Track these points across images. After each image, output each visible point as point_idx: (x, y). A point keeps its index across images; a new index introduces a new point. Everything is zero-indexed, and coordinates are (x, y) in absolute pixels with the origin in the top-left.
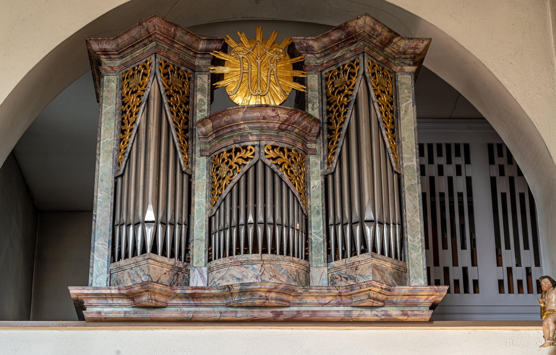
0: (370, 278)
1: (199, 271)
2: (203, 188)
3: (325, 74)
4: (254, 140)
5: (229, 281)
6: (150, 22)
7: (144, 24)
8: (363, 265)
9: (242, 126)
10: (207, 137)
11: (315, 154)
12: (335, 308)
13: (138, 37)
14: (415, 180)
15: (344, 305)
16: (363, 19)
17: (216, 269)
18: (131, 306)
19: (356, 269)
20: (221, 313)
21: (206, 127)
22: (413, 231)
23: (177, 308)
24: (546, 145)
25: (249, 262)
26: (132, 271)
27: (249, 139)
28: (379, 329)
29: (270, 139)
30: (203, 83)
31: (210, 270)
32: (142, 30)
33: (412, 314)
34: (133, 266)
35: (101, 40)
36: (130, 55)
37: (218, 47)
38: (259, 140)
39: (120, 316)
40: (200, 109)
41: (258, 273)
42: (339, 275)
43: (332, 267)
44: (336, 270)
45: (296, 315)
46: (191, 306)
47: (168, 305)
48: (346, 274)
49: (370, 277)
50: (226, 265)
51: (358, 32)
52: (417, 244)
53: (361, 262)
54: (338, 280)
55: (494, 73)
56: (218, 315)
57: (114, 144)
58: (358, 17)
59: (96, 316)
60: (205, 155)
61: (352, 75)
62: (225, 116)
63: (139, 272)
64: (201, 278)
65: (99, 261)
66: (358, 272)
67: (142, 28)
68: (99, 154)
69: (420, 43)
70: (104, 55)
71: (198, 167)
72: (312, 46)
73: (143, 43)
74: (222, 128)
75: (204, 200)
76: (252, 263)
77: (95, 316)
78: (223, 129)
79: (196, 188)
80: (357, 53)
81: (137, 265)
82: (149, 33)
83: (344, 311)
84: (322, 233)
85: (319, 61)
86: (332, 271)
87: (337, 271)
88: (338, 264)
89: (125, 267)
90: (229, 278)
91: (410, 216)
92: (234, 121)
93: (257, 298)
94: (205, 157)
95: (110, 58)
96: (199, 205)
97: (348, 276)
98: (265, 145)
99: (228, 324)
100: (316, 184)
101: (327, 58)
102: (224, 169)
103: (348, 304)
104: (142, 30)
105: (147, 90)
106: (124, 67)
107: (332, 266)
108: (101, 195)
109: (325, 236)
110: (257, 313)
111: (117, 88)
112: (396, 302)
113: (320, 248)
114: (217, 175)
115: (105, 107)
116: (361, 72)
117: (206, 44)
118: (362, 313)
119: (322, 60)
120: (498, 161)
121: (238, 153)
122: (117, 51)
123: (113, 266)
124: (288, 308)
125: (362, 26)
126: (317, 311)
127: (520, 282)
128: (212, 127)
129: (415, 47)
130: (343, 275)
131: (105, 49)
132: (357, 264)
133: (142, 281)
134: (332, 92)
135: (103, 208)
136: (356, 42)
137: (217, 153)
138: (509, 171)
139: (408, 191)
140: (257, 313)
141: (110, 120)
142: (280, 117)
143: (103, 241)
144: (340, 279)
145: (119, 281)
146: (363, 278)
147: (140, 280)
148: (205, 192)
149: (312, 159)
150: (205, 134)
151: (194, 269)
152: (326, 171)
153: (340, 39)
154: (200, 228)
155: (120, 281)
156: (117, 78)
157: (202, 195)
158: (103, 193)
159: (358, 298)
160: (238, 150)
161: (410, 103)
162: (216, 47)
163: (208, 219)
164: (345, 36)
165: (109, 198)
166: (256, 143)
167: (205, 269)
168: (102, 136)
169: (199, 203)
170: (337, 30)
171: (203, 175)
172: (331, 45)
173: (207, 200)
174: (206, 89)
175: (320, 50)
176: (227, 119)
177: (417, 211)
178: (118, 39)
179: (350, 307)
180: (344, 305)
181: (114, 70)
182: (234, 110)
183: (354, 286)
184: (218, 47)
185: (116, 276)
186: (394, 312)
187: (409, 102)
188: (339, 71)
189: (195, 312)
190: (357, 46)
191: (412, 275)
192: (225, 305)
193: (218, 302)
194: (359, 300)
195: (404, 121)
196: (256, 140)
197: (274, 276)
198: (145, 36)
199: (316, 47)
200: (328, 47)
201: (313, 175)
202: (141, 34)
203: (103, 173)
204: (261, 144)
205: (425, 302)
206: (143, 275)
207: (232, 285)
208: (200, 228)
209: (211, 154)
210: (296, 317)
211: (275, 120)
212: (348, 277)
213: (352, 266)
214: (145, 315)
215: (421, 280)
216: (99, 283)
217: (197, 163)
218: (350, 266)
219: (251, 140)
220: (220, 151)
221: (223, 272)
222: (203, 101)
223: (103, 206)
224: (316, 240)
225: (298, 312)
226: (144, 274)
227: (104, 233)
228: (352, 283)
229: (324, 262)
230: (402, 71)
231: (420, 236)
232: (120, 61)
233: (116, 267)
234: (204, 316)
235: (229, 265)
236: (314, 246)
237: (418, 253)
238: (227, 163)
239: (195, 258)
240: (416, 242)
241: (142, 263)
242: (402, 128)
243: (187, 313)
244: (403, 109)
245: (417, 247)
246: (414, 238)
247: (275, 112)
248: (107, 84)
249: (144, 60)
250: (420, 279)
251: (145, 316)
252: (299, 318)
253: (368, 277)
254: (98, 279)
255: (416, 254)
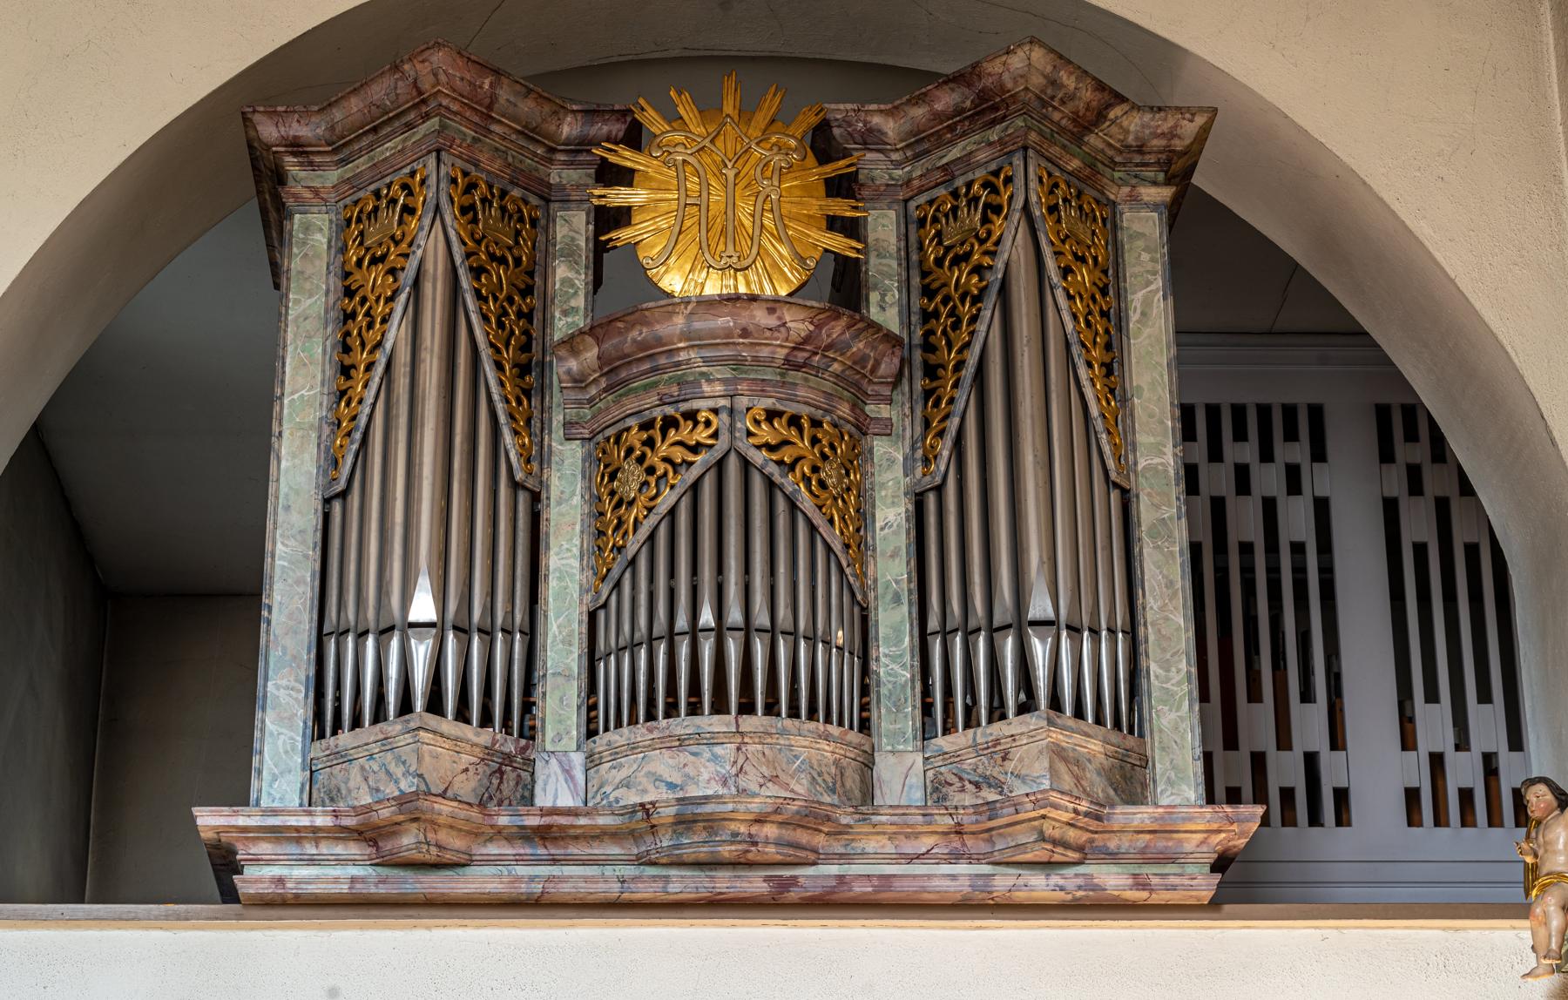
0: (1042, 784)
1: (560, 762)
2: (573, 529)
3: (917, 207)
4: (717, 394)
5: (645, 791)
6: (423, 62)
7: (407, 67)
8: (1025, 748)
9: (683, 356)
10: (583, 385)
11: (890, 435)
12: (946, 869)
13: (388, 103)
14: (1170, 506)
15: (969, 858)
16: (1022, 54)
17: (609, 758)
18: (368, 863)
19: (1004, 759)
20: (623, 882)
21: (582, 357)
22: (1164, 650)
23: (499, 868)
24: (1540, 410)
25: (703, 739)
26: (371, 762)
27: (703, 392)
28: (1068, 927)
29: (763, 391)
30: (572, 234)
31: (592, 761)
32: (400, 84)
33: (1162, 885)
34: (376, 751)
35: (286, 112)
36: (366, 156)
37: (614, 133)
38: (732, 393)
39: (337, 891)
40: (565, 307)
41: (728, 768)
42: (956, 775)
43: (937, 751)
44: (949, 761)
45: (835, 887)
46: (538, 861)
47: (474, 858)
48: (975, 771)
49: (1044, 781)
50: (638, 747)
51: (1009, 91)
52: (1175, 689)
53: (1017, 737)
54: (952, 788)
55: (1392, 207)
56: (616, 887)
57: (321, 404)
58: (1009, 47)
59: (270, 891)
60: (579, 436)
61: (992, 212)
62: (633, 326)
63: (392, 767)
64: (566, 782)
65: (279, 734)
66: (1010, 766)
67: (401, 79)
68: (280, 433)
69: (1186, 122)
70: (294, 154)
71: (558, 470)
72: (879, 131)
73: (404, 120)
74: (627, 360)
75: (576, 564)
76: (712, 741)
77: (267, 889)
78: (629, 363)
79: (552, 530)
80: (1008, 149)
81: (387, 748)
82: (420, 93)
83: (970, 875)
84: (908, 657)
85: (900, 172)
86: (936, 765)
87: (951, 763)
88: (952, 743)
89: (352, 752)
90: (646, 783)
91: (1155, 607)
92: (659, 341)
93: (724, 838)
94: (578, 442)
95: (311, 164)
96: (560, 579)
97: (980, 776)
98: (748, 409)
99: (642, 913)
100: (891, 518)
101: (923, 164)
102: (632, 476)
103: (981, 857)
104: (400, 84)
105: (414, 252)
106: (350, 189)
107: (936, 748)
108: (284, 549)
109: (917, 664)
110: (724, 883)
111: (329, 247)
112: (1116, 851)
113: (903, 700)
114: (612, 493)
115: (297, 302)
116: (1019, 203)
117: (580, 124)
118: (1021, 881)
119: (909, 168)
120: (1405, 452)
121: (672, 432)
122: (329, 145)
123: (318, 749)
124: (813, 868)
125: (1020, 72)
126: (894, 876)
127: (1466, 796)
128: (599, 358)
129: (1171, 133)
130: (968, 774)
131: (295, 137)
132: (1007, 743)
133: (400, 790)
134: (936, 259)
135: (292, 586)
136: (1004, 118)
137: (611, 432)
138: (1436, 482)
139: (1151, 537)
140: (724, 883)
141: (309, 337)
142: (788, 329)
143: (292, 679)
144: (960, 785)
145: (334, 793)
146: (1024, 782)
147: (394, 788)
148: (577, 541)
149: (880, 447)
150: (578, 377)
151: (547, 758)
152: (920, 481)
153: (959, 111)
154: (563, 642)
155: (339, 790)
156: (331, 221)
157: (568, 550)
158: (292, 542)
159: (1009, 839)
160: (670, 423)
161: (1157, 290)
162: (610, 131)
163: (585, 618)
164: (972, 102)
165: (306, 557)
166: (722, 402)
167: (578, 759)
168: (287, 383)
169: (561, 572)
170: (952, 85)
171: (573, 494)
172: (933, 128)
173: (585, 562)
174: (581, 250)
175: (902, 141)
176: (640, 334)
177: (1175, 593)
178: (334, 111)
179: (988, 863)
180: (971, 859)
181: (322, 198)
182: (661, 310)
183: (998, 805)
184: (614, 133)
185: (327, 777)
186: (1112, 879)
187: (1153, 287)
188: (957, 200)
189: (550, 879)
190: (1007, 128)
191: (1162, 775)
192: (634, 858)
193: (614, 850)
194: (1013, 844)
195: (1139, 340)
196: (722, 393)
197: (774, 779)
198: (408, 102)
199: (890, 133)
200: (924, 131)
201: (883, 493)
202: (397, 95)
203: (291, 488)
204: (736, 406)
205: (1199, 850)
206: (404, 775)
207: (653, 803)
208: (563, 642)
209: (594, 434)
210: (835, 892)
211: (777, 339)
212: (981, 780)
213: (993, 750)
214: (408, 886)
215: (1187, 789)
216: (280, 798)
217: (555, 459)
218: (988, 748)
219: (707, 395)
220: (620, 426)
221: (629, 767)
222: (573, 285)
223: (290, 581)
224: (890, 675)
225: (841, 878)
226: (407, 773)
227: (294, 657)
228: (992, 796)
229: (915, 738)
230: (1134, 199)
231: (1183, 665)
232: (339, 171)
233: (328, 752)
234: (574, 890)
235: (644, 747)
236: (886, 692)
237: (1179, 714)
238: (641, 459)
239: (549, 727)
240: (1174, 681)
241: (399, 741)
242: (1134, 361)
243: (526, 883)
244: (1135, 308)
245: (1177, 697)
246: (1168, 670)
247: (776, 315)
248: (301, 236)
249: (407, 170)
250: (1184, 787)
251: (409, 891)
252: (844, 895)
253: (1038, 781)
254: (276, 786)
255: (1173, 715)
